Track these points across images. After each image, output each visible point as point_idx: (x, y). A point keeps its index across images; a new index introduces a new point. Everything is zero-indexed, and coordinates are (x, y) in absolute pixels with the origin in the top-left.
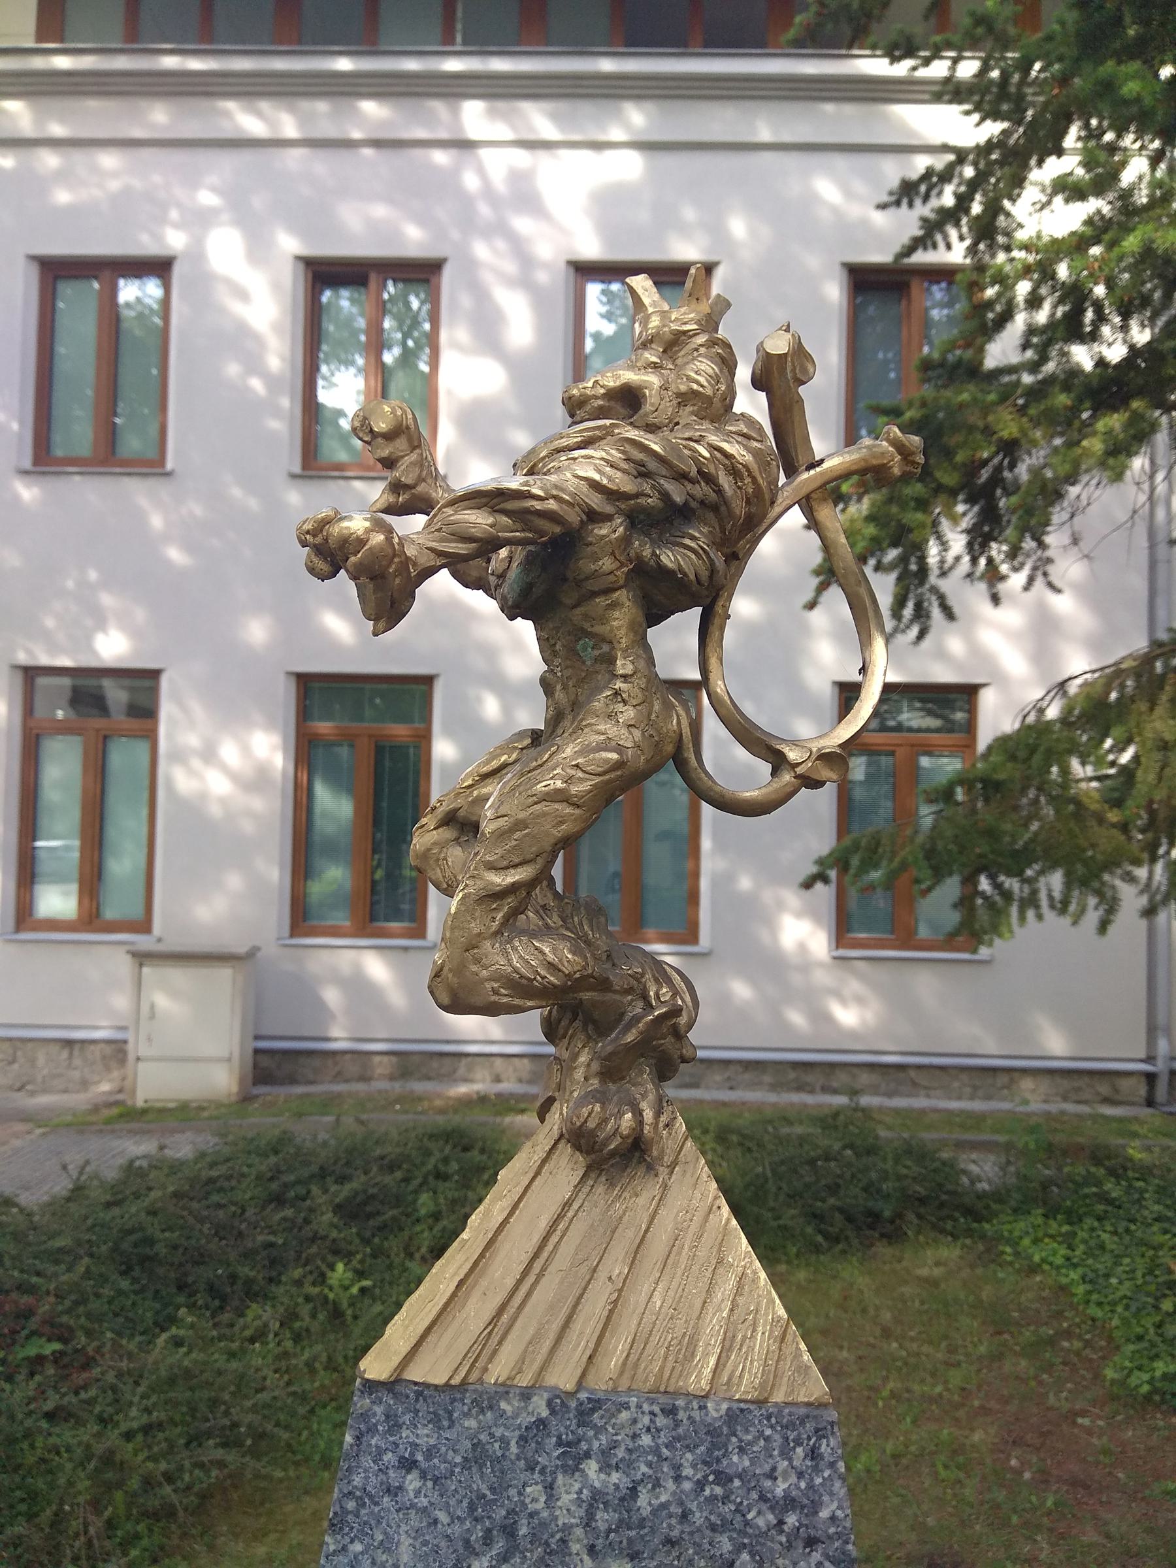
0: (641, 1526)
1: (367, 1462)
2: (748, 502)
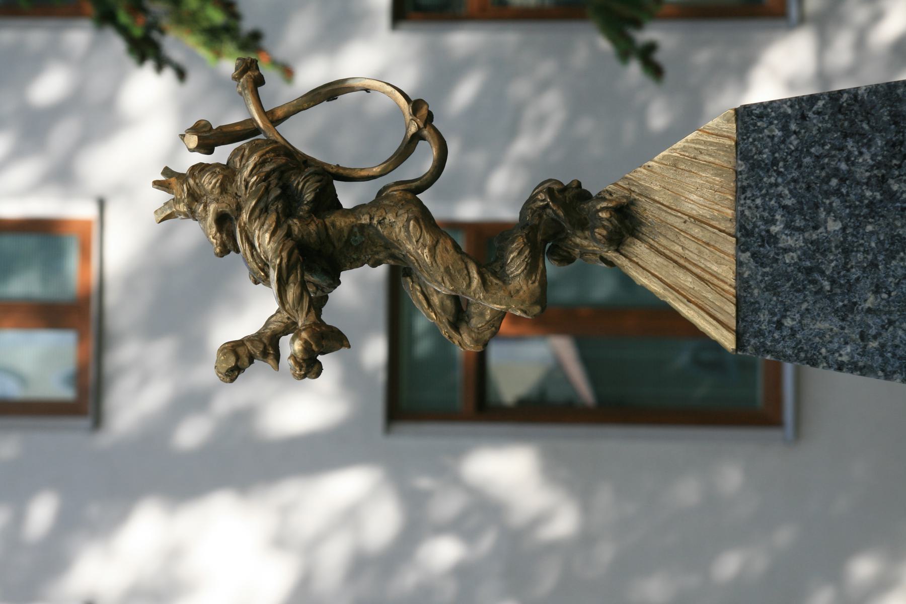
0: (801, 203)
1: (779, 347)
2: (278, 155)
